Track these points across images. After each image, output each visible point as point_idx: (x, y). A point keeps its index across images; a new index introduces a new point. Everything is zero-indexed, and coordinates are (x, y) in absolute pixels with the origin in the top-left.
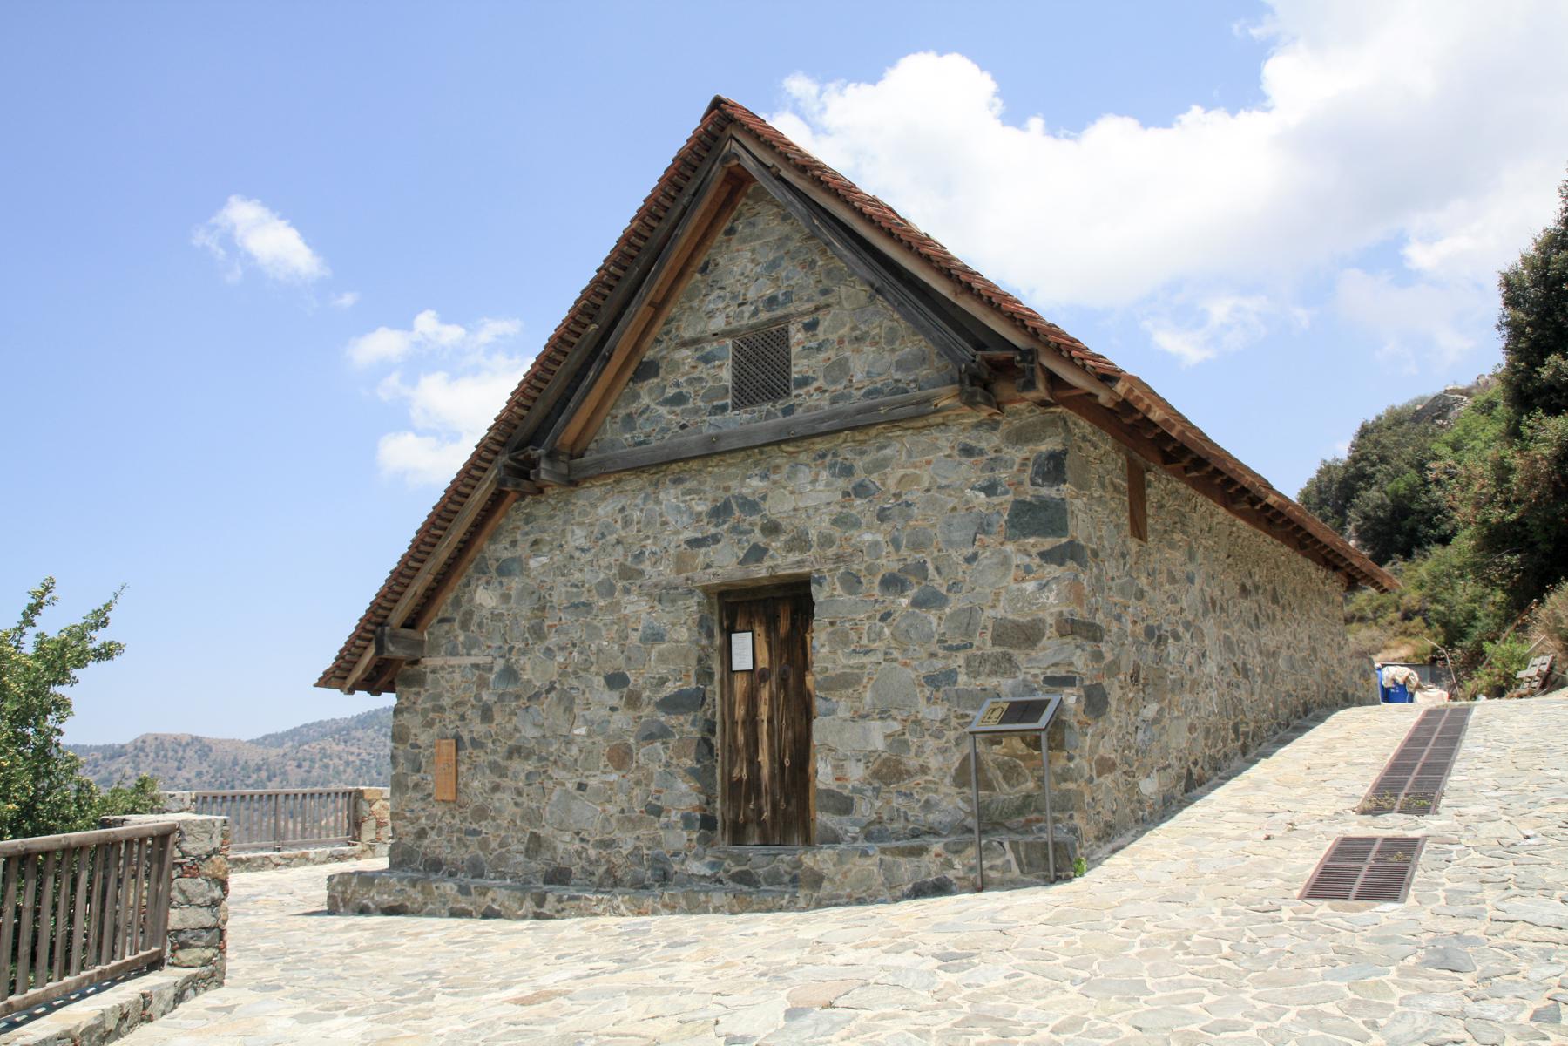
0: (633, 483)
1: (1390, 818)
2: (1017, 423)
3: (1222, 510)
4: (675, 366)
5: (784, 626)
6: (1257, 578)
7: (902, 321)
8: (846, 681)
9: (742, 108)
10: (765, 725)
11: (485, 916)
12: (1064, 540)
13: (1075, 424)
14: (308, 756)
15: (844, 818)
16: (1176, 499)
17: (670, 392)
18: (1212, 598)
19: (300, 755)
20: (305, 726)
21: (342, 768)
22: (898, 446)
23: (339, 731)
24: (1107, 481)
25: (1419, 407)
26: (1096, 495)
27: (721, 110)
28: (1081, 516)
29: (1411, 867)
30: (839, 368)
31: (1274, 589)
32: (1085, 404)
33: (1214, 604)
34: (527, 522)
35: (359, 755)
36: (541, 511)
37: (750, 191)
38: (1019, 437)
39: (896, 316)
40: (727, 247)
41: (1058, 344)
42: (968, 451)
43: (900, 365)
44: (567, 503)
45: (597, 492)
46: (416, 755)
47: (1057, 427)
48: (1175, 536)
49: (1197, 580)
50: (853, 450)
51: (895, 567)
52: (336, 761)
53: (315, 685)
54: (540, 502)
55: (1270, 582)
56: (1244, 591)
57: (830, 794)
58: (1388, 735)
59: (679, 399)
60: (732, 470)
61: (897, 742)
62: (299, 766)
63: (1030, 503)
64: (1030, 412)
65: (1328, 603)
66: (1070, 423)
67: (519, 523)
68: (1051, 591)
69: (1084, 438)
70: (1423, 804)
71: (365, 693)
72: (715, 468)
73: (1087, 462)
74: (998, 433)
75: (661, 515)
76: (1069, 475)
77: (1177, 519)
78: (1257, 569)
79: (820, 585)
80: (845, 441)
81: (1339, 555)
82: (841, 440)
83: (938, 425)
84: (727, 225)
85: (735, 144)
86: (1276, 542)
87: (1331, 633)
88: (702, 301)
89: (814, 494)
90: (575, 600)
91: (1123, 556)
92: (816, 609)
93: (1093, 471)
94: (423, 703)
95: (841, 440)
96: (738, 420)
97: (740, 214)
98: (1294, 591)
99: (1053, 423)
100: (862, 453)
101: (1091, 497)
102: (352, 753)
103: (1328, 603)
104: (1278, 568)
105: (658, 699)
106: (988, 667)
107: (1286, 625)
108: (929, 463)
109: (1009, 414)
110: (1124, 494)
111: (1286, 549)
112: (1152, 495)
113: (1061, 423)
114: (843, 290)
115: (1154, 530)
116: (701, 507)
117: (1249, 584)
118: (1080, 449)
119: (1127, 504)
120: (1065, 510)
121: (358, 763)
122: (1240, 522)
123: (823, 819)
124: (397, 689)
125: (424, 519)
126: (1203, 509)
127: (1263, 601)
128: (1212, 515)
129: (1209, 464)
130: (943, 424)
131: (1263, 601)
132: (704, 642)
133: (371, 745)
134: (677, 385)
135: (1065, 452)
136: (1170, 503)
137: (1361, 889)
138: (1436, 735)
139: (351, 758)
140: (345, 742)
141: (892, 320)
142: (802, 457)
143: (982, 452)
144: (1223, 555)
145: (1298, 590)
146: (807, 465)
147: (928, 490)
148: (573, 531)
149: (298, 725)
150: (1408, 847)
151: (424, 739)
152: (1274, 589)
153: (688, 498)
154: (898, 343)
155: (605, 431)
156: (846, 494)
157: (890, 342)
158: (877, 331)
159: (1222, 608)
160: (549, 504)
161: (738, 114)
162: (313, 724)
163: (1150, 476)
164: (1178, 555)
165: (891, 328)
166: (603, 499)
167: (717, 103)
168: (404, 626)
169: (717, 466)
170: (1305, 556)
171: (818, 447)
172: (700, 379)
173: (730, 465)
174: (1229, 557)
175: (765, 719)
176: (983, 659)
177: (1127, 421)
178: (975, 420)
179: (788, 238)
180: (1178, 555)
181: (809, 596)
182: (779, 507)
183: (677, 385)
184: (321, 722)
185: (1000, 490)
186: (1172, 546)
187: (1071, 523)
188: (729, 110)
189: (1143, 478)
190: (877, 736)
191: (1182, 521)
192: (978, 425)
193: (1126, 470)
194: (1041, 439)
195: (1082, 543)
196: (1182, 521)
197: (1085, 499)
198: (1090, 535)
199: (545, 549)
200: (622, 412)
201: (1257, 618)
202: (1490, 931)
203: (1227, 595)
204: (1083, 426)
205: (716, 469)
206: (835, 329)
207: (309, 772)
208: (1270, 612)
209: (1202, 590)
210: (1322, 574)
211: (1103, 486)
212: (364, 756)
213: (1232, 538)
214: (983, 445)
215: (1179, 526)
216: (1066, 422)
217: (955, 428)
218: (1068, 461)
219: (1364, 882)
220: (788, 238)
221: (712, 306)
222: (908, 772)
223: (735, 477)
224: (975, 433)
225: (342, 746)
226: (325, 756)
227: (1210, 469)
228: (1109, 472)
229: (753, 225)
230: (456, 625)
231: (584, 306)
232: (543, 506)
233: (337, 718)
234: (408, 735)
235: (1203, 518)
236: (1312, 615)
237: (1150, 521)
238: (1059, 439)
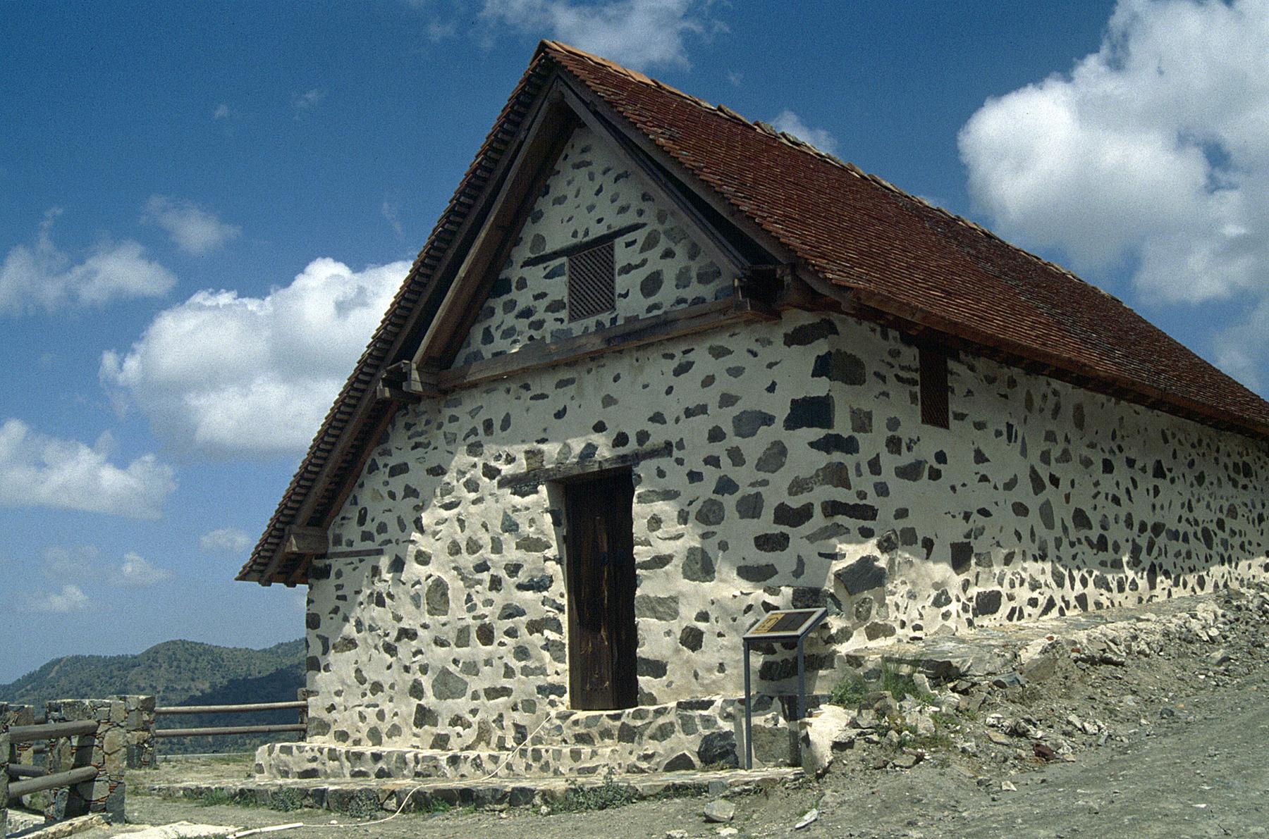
27: (547, 53)
53: (237, 579)
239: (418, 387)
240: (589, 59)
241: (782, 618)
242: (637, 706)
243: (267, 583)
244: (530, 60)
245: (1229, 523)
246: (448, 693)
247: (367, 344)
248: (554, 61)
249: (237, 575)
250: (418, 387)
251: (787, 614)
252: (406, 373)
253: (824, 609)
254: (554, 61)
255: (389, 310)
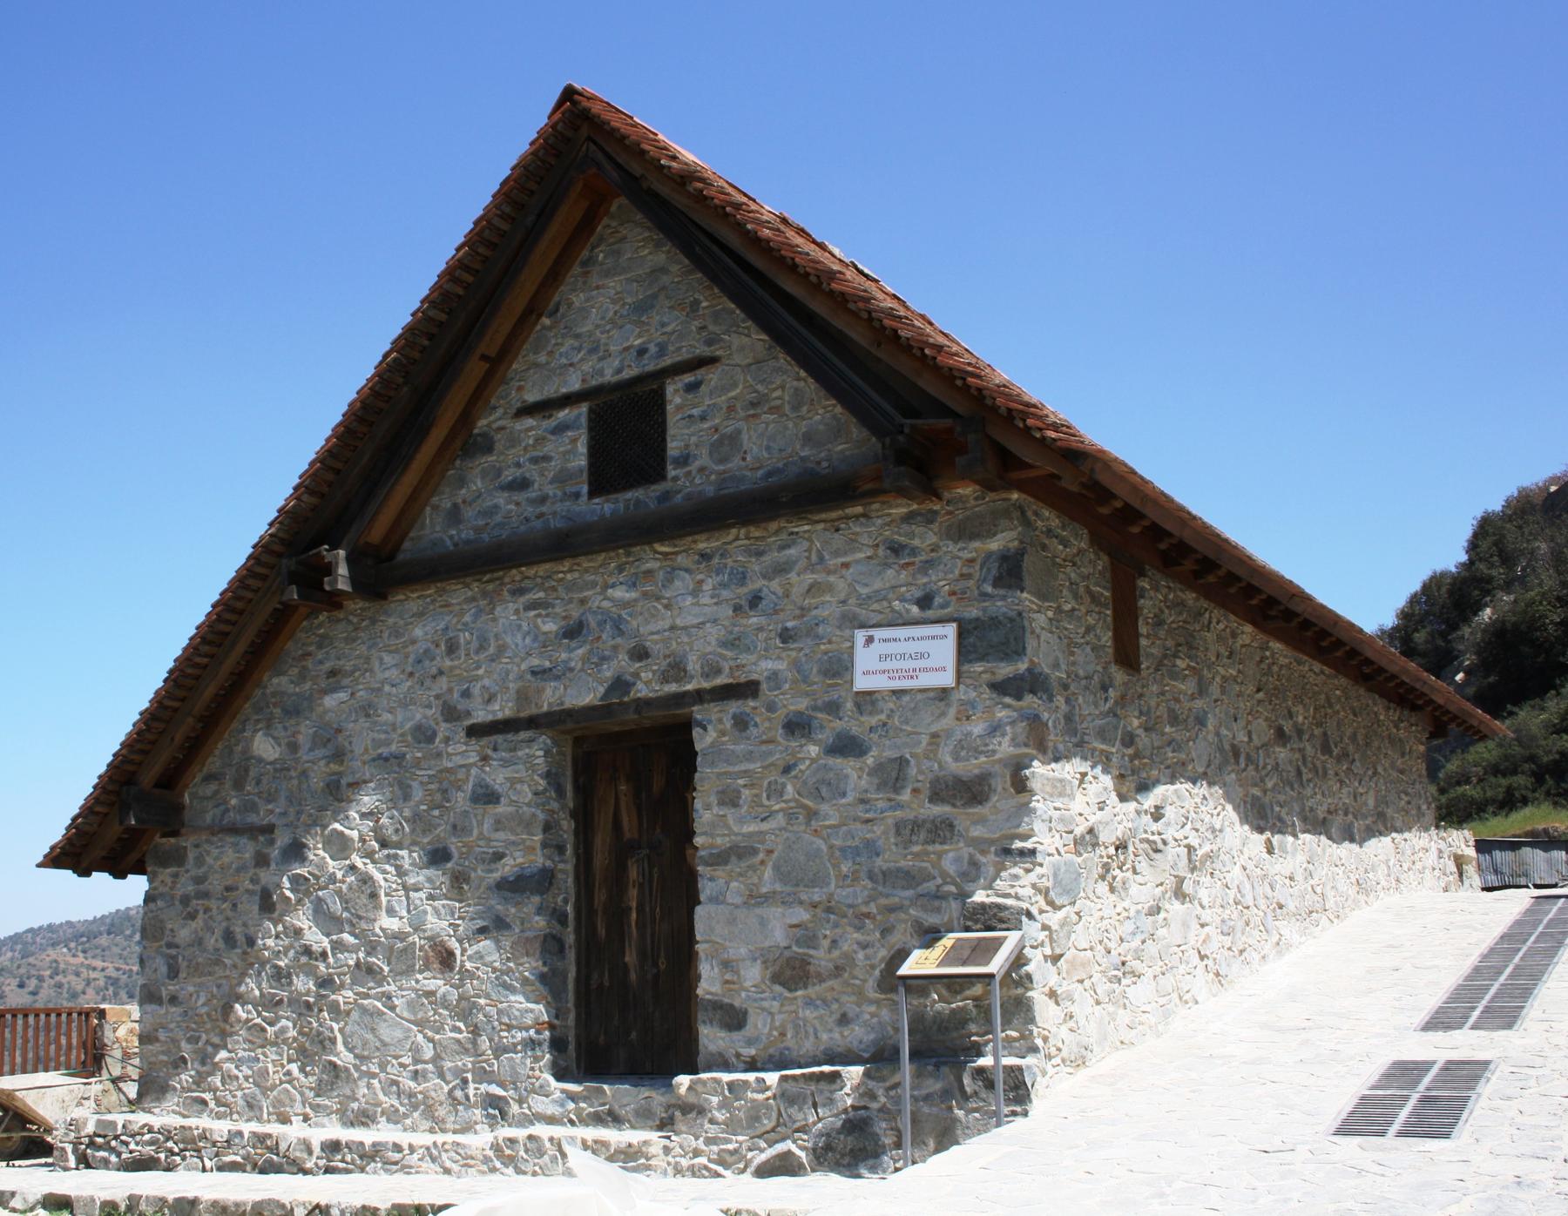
0: (459, 594)
1: (1457, 1036)
2: (960, 515)
3: (1248, 628)
4: (513, 441)
5: (658, 783)
6: (1300, 719)
7: (811, 380)
8: (740, 852)
9: (602, 101)
10: (634, 915)
11: (263, 1171)
12: (1023, 666)
13: (1036, 514)
14: (33, 972)
15: (736, 1035)
16: (1180, 613)
17: (509, 475)
18: (1233, 746)
19: (22, 971)
20: (31, 930)
21: (79, 988)
22: (806, 544)
23: (77, 937)
24: (1082, 590)
25: (1553, 489)
26: (1067, 607)
27: (574, 103)
28: (1045, 636)
29: (1474, 1097)
30: (727, 444)
31: (1325, 734)
32: (1047, 491)
33: (1236, 754)
34: (320, 647)
35: (103, 970)
36: (340, 630)
37: (613, 208)
38: (964, 532)
39: (803, 374)
40: (585, 283)
41: (1010, 410)
42: (896, 549)
43: (808, 438)
44: (374, 621)
45: (413, 606)
46: (174, 958)
47: (1011, 519)
48: (1179, 662)
49: (1211, 723)
50: (748, 551)
51: (802, 704)
52: (71, 978)
53: (39, 866)
54: (339, 620)
55: (1319, 725)
56: (1281, 737)
57: (717, 1006)
58: (1476, 930)
59: (522, 484)
60: (589, 578)
61: (807, 936)
62: (21, 986)
63: (977, 619)
64: (976, 499)
65: (1403, 755)
66: (1029, 514)
67: (312, 648)
68: (1003, 735)
69: (1049, 532)
70: (1504, 1015)
71: (106, 875)
72: (565, 571)
73: (1055, 564)
74: (935, 526)
75: (496, 636)
76: (1027, 582)
77: (1182, 640)
78: (1300, 708)
79: (705, 729)
80: (737, 539)
81: (1413, 689)
82: (731, 537)
83: (857, 517)
84: (585, 253)
85: (593, 147)
86: (1327, 670)
87: (1407, 794)
88: (551, 353)
89: (696, 610)
90: (384, 751)
91: (1105, 688)
92: (699, 759)
93: (1061, 576)
94: (186, 887)
95: (731, 537)
96: (606, 507)
97: (601, 240)
98: (1353, 738)
99: (1006, 513)
100: (760, 554)
101: (1059, 610)
102: (94, 969)
103: (1403, 755)
104: (1331, 706)
105: (491, 881)
106: (923, 835)
107: (1341, 782)
108: (846, 565)
109: (948, 503)
110: (1106, 606)
111: (1343, 681)
112: (1147, 606)
113: (1016, 514)
114: (736, 341)
115: (1148, 655)
116: (550, 626)
117: (1287, 727)
118: (1044, 547)
119: (1109, 619)
120: (1023, 628)
121: (102, 983)
122: (1276, 645)
123: (711, 1037)
124: (149, 869)
125: (185, 642)
126: (1221, 626)
127: (1309, 750)
128: (1234, 635)
129: (1219, 567)
130: (864, 515)
131: (1309, 750)
132: (555, 805)
133: (121, 957)
134: (518, 465)
135: (1021, 553)
136: (1170, 617)
137: (1406, 1123)
138: (1540, 929)
139: (93, 975)
140: (84, 952)
141: (799, 379)
142: (681, 560)
143: (914, 552)
144: (1251, 688)
145: (1360, 737)
146: (687, 570)
147: (844, 602)
148: (381, 659)
149: (21, 930)
150: (1467, 1074)
151: (184, 934)
152: (1325, 734)
153: (533, 613)
154: (805, 409)
155: (423, 527)
156: (737, 609)
157: (796, 408)
158: (777, 393)
159: (1248, 758)
160: (350, 622)
161: (596, 108)
162: (40, 928)
163: (1144, 583)
164: (1189, 686)
165: (796, 389)
166: (420, 615)
167: (569, 94)
168: (157, 785)
169: (571, 571)
170: (1369, 690)
171: (701, 546)
172: (546, 458)
173: (586, 571)
174: (1259, 690)
175: (634, 904)
176: (916, 825)
177: (1104, 511)
178: (905, 510)
179: (663, 270)
180: (1189, 686)
181: (691, 743)
182: (651, 627)
183: (518, 465)
184: (50, 926)
185: (938, 600)
186: (1175, 675)
187: (1031, 644)
188: (585, 103)
189: (1134, 587)
190: (778, 925)
191: (1188, 644)
192: (909, 518)
193: (1108, 575)
194: (992, 534)
195: (1047, 670)
196: (1188, 644)
197: (1050, 614)
198: (1057, 658)
199: (346, 682)
200: (447, 504)
201: (1299, 773)
202: (1559, 1176)
203: (1256, 741)
204: (1049, 518)
205: (569, 577)
206: (725, 389)
207: (34, 993)
208: (1318, 763)
209: (1218, 734)
210: (1395, 715)
211: (1076, 596)
212: (111, 972)
213: (1263, 666)
214: (916, 542)
215: (1184, 649)
216: (1023, 513)
217: (879, 521)
218: (1027, 562)
219: (1412, 1114)
220: (663, 270)
221: (564, 361)
222: (819, 975)
223: (594, 584)
224: (905, 527)
225: (81, 958)
226: (56, 973)
227: (1221, 573)
228: (1086, 578)
229: (618, 253)
230: (228, 784)
231: (395, 360)
232: (340, 626)
233: (74, 919)
234: (162, 929)
235: (1220, 638)
236: (1380, 770)
237: (1143, 642)
238: (1013, 534)
239: (343, 585)
240: (801, 232)
241: (952, 947)
242: (697, 1073)
243: (85, 873)
244: (549, 110)
245: (854, 774)
246: (378, 1044)
247: (269, 520)
248: (627, 142)
249: (40, 859)
250: (343, 585)
251: (959, 940)
252: (330, 563)
253: (1020, 933)
254: (627, 142)
255: (307, 471)
